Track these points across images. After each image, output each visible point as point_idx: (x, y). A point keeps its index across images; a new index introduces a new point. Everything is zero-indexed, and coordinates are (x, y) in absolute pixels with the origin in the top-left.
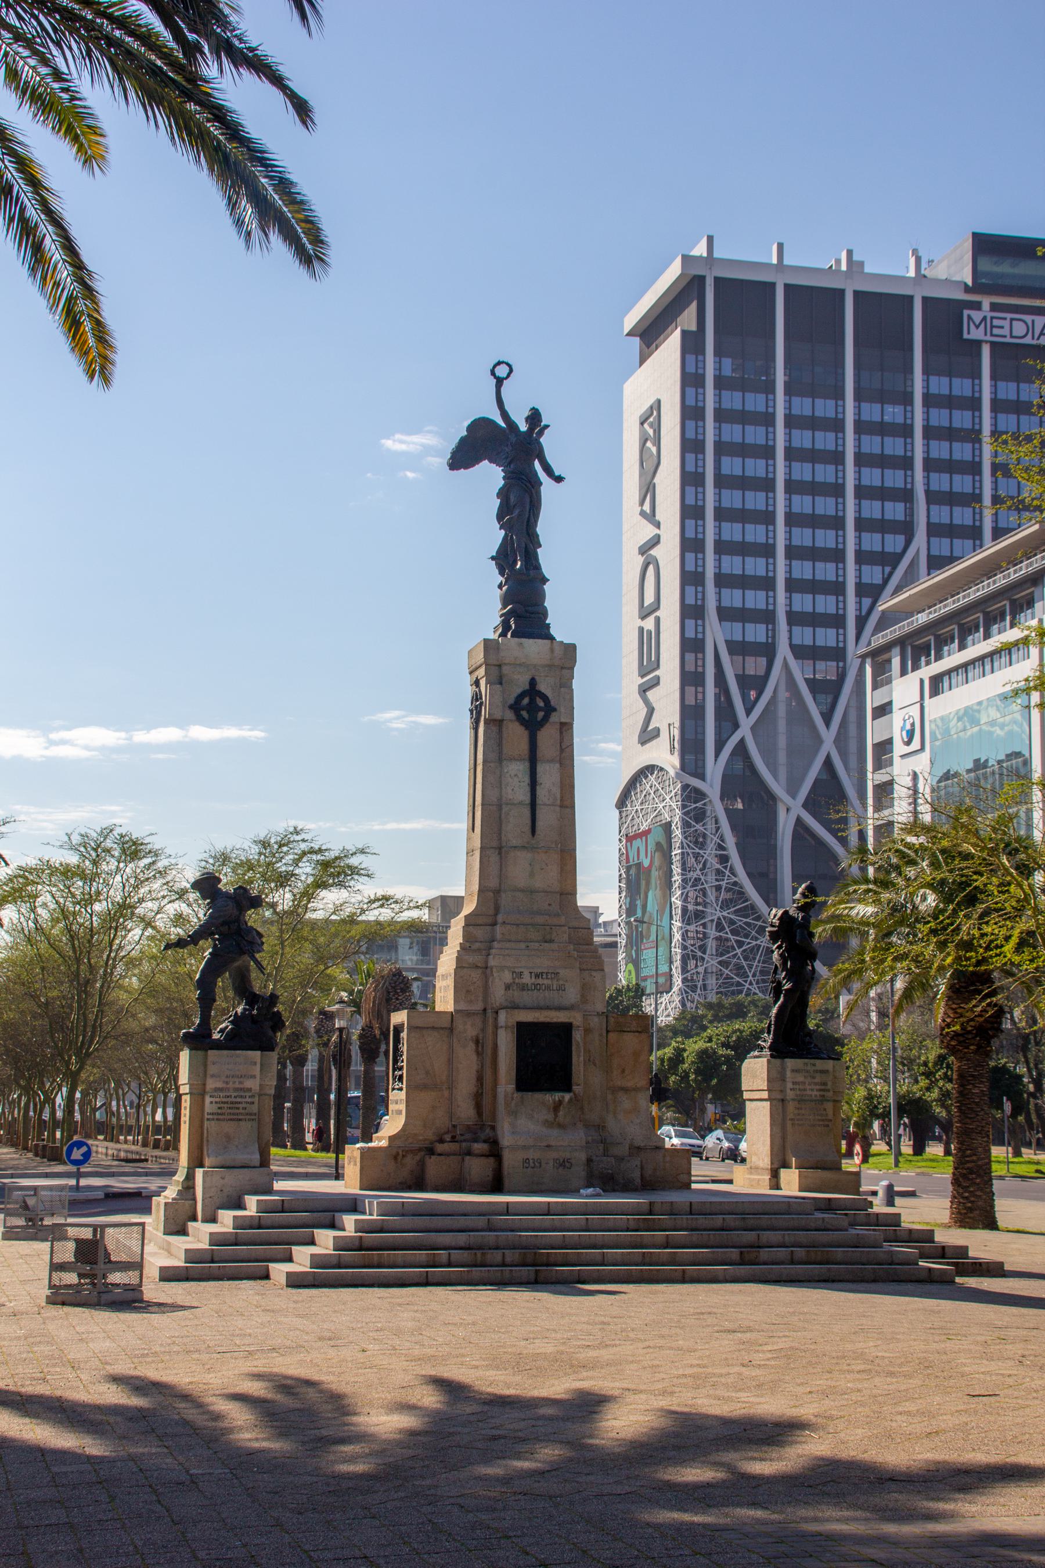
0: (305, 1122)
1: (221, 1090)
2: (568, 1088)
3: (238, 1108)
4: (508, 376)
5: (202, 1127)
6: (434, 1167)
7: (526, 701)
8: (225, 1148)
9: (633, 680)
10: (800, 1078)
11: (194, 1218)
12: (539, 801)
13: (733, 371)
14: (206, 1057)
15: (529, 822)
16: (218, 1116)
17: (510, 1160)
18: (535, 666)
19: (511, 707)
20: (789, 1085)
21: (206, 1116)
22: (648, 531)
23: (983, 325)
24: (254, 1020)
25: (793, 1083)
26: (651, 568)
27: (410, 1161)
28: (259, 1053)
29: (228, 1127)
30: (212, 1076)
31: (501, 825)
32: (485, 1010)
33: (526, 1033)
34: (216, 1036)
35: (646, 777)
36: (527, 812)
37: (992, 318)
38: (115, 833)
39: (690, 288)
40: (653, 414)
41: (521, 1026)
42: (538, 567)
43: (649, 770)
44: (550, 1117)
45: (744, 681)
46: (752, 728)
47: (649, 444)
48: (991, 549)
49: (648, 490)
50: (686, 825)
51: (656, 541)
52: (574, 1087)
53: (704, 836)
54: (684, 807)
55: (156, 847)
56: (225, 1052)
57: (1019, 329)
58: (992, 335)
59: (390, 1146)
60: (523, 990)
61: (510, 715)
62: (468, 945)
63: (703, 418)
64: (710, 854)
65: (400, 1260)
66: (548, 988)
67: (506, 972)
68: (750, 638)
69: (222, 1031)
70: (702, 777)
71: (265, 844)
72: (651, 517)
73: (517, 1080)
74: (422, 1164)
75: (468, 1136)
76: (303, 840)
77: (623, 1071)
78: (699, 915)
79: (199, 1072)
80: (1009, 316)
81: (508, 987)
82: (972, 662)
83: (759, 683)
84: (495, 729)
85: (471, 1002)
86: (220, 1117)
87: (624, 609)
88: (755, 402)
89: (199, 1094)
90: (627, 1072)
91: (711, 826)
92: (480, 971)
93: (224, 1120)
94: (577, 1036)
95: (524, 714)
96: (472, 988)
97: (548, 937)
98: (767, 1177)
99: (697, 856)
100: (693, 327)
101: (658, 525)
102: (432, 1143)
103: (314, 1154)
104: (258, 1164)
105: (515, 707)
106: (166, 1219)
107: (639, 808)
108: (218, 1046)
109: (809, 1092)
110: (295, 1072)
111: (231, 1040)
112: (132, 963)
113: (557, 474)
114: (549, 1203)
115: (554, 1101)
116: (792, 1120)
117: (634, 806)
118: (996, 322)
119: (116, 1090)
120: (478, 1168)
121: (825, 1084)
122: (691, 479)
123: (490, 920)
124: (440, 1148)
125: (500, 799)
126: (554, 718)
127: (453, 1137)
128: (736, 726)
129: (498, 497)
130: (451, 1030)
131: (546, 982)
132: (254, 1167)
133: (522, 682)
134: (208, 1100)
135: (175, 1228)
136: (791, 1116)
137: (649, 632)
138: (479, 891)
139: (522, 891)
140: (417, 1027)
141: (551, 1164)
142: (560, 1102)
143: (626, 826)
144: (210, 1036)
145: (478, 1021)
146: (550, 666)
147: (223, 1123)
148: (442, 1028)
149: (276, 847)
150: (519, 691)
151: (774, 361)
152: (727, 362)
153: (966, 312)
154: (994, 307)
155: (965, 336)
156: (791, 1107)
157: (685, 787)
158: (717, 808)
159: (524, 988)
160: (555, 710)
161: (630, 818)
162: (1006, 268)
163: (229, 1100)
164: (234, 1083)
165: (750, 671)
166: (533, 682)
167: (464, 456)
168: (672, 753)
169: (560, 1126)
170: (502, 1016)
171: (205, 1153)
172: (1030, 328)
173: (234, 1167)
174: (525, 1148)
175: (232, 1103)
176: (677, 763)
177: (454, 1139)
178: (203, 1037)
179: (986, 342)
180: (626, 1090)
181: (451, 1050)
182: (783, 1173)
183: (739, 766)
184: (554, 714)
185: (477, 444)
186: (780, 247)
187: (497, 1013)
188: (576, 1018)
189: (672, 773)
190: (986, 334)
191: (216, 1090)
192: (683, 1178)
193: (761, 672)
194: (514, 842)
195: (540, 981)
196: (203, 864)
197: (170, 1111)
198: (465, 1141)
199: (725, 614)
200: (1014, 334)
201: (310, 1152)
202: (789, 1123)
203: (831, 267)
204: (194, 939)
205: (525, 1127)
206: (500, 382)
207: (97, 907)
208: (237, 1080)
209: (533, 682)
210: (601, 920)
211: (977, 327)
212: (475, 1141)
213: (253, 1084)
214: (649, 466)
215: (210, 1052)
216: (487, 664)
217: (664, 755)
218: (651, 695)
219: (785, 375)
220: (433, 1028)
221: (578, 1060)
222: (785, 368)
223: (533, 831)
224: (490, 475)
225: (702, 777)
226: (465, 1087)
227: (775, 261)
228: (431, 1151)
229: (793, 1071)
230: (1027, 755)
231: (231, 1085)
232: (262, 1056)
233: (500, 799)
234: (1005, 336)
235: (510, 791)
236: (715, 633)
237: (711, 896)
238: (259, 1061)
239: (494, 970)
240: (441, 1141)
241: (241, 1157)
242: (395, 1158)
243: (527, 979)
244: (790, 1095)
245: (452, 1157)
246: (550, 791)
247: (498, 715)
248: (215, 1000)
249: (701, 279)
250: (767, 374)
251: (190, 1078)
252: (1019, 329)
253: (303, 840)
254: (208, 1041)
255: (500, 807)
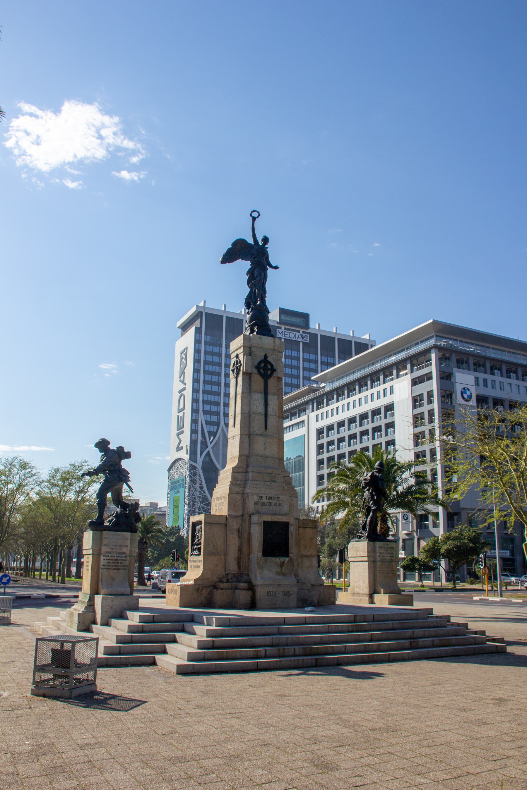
1: (109, 553)
2: (287, 555)
5: (98, 572)
6: (219, 596)
7: (262, 365)
9: (175, 432)
10: (382, 551)
12: (268, 413)
14: (101, 535)
15: (264, 423)
16: (107, 567)
17: (260, 592)
19: (256, 367)
20: (378, 554)
22: (182, 386)
25: (380, 553)
26: (182, 397)
27: (205, 592)
28: (130, 533)
30: (105, 545)
31: (250, 424)
32: (243, 515)
33: (268, 526)
34: (106, 524)
36: (263, 418)
38: (18, 459)
39: (198, 315)
40: (185, 351)
41: (265, 523)
42: (265, 305)
43: (179, 459)
44: (279, 570)
45: (210, 433)
46: (212, 448)
47: (183, 360)
48: (302, 389)
49: (182, 373)
50: (190, 477)
51: (184, 389)
52: (290, 555)
53: (196, 480)
54: (190, 471)
55: (33, 465)
56: (112, 532)
57: (292, 336)
59: (195, 584)
60: (263, 505)
61: (255, 371)
62: (234, 482)
63: (200, 353)
64: (197, 486)
65: (238, 655)
66: (274, 505)
67: (255, 496)
68: (212, 420)
69: (110, 521)
70: (196, 462)
71: (74, 466)
72: (183, 382)
73: (263, 551)
74: (211, 594)
75: (234, 579)
77: (306, 547)
78: (194, 505)
79: (97, 543)
80: (289, 332)
81: (256, 504)
82: (295, 425)
83: (214, 434)
84: (247, 377)
85: (236, 511)
86: (109, 567)
87: (173, 410)
88: (216, 350)
89: (96, 554)
90: (307, 547)
91: (198, 478)
92: (240, 495)
93: (110, 569)
94: (292, 529)
95: (262, 371)
96: (236, 504)
97: (273, 479)
98: (367, 598)
99: (193, 487)
100: (199, 326)
101: (185, 384)
102: (215, 583)
105: (258, 367)
108: (108, 529)
109: (386, 558)
110: (68, 551)
111: (115, 526)
112: (18, 510)
113: (274, 265)
114: (305, 617)
115: (281, 561)
116: (379, 571)
117: (174, 470)
119: (6, 555)
120: (243, 596)
121: (392, 554)
122: (196, 371)
123: (244, 471)
124: (222, 585)
125: (250, 411)
126: (275, 374)
127: (228, 580)
128: (207, 447)
130: (226, 525)
131: (273, 501)
132: (127, 595)
133: (260, 356)
134: (102, 558)
136: (378, 569)
137: (181, 417)
138: (240, 456)
139: (261, 456)
140: (209, 523)
141: (281, 594)
142: (284, 562)
144: (103, 523)
145: (239, 520)
146: (274, 350)
147: (110, 571)
148: (222, 524)
150: (259, 360)
151: (222, 338)
153: (277, 329)
154: (285, 329)
156: (379, 564)
157: (191, 465)
158: (200, 472)
159: (263, 504)
160: (275, 370)
163: (113, 558)
164: (116, 549)
165: (212, 430)
166: (266, 357)
167: (229, 257)
168: (187, 454)
169: (284, 574)
170: (255, 518)
171: (100, 586)
172: (295, 336)
174: (268, 585)
175: (115, 560)
176: (188, 457)
177: (228, 581)
180: (307, 556)
181: (226, 536)
182: (376, 596)
183: (207, 459)
184: (275, 372)
186: (225, 306)
187: (250, 516)
188: (292, 521)
189: (187, 460)
191: (107, 552)
192: (332, 599)
193: (215, 431)
194: (257, 432)
195: (270, 501)
196: (50, 472)
197: (18, 563)
198: (233, 582)
199: (205, 412)
201: (73, 579)
202: (378, 572)
204: (96, 472)
205: (266, 575)
207: (10, 486)
208: (118, 548)
209: (266, 357)
210: (158, 507)
212: (239, 581)
213: (126, 550)
214: (183, 366)
215: (104, 532)
216: (244, 346)
217: (185, 455)
220: (217, 523)
221: (292, 541)
223: (266, 428)
225: (196, 462)
226: (233, 553)
227: (223, 309)
228: (215, 587)
229: (379, 547)
230: (303, 456)
233: (250, 411)
235: (255, 407)
236: (202, 418)
237: (197, 499)
238: (129, 538)
239: (249, 495)
240: (221, 581)
241: (121, 590)
242: (198, 590)
243: (264, 500)
244: (378, 559)
245: (228, 590)
246: (273, 409)
247: (250, 371)
248: (106, 505)
249: (202, 313)
251: (92, 546)
252: (292, 336)
255: (250, 415)
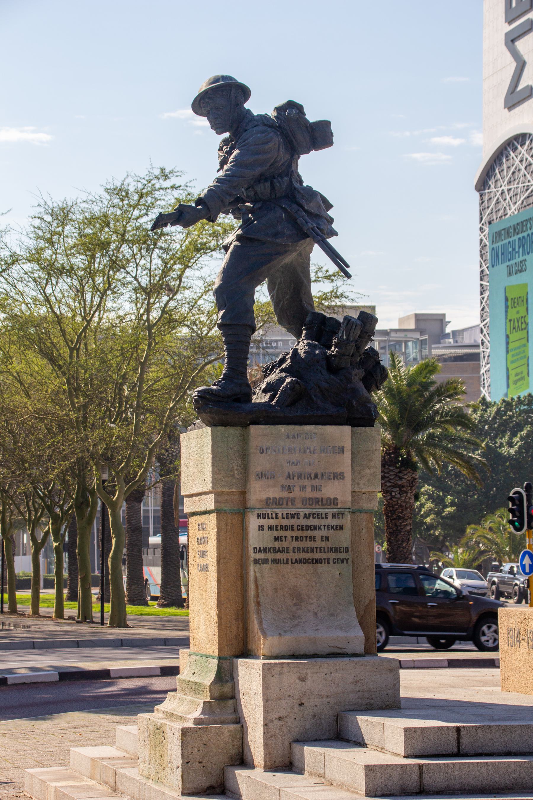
0: (146, 570)
1: (278, 502)
3: (313, 539)
5: (243, 576)
8: (294, 617)
11: (243, 760)
14: (245, 440)
16: (274, 555)
21: (252, 555)
24: (331, 366)
28: (347, 429)
29: (297, 576)
30: (261, 476)
34: (260, 398)
35: (515, 149)
56: (283, 429)
69: (271, 388)
71: (121, 193)
76: (173, 187)
86: (279, 556)
89: (233, 512)
103: (160, 609)
104: (361, 649)
106: (186, 762)
107: (505, 189)
108: (266, 416)
111: (293, 404)
117: (500, 185)
134: (253, 523)
135: (203, 782)
143: (488, 211)
144: (248, 396)
147: (286, 569)
149: (136, 197)
161: (494, 201)
164: (303, 488)
171: (255, 626)
173: (315, 656)
175: (301, 528)
178: (237, 400)
191: (269, 502)
196: (37, 222)
201: (154, 608)
208: (306, 482)
210: (448, 330)
213: (339, 491)
215: (254, 429)
218: (521, 45)
231: (297, 493)
232: (353, 433)
238: (347, 444)
241: (329, 636)
251: (215, 482)
253: (173, 187)
254: (247, 407)
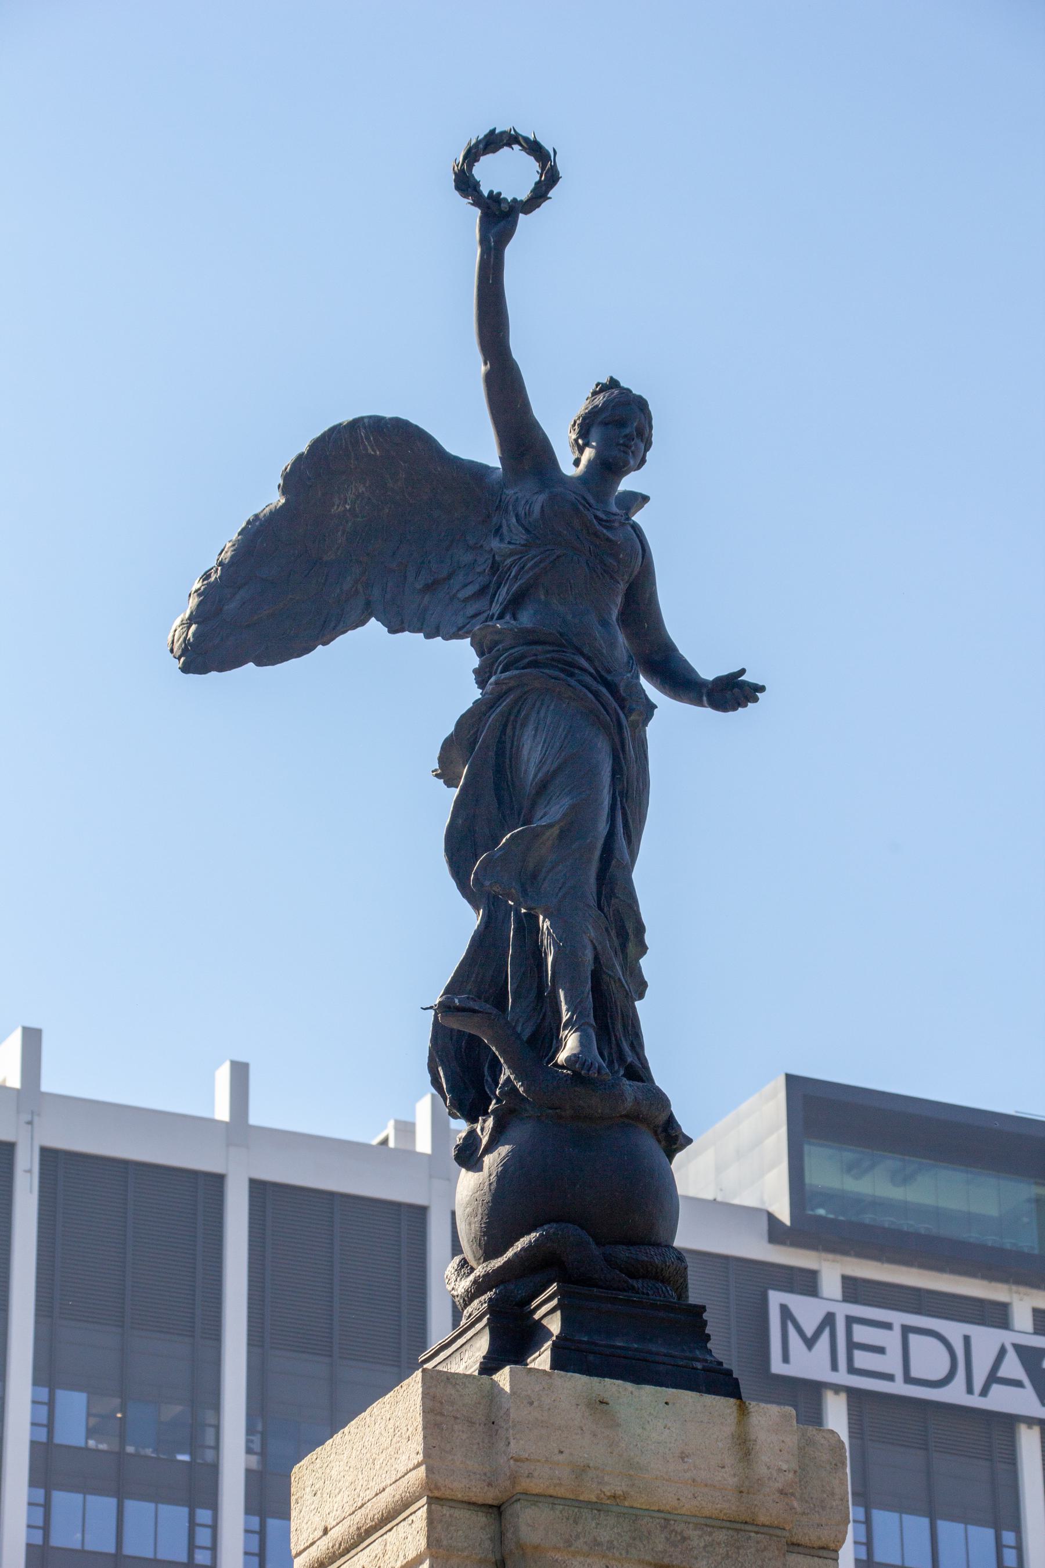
4: (540, 194)
13: (90, 1433)
18: (666, 1518)
23: (826, 1335)
37: (850, 1320)
57: (929, 1358)
58: (852, 1370)
80: (899, 1318)
113: (708, 671)
118: (861, 1334)
129: (446, 773)
151: (216, 1405)
152: (73, 1405)
153: (776, 1298)
154: (855, 1290)
155: (777, 1367)
162: (877, 1185)
167: (260, 606)
172: (959, 1361)
179: (837, 1389)
185: (341, 541)
186: (240, 1073)
190: (834, 1367)
200: (914, 1373)
203: (385, 1142)
206: (498, 219)
211: (810, 1343)
219: (249, 1451)
222: (250, 1430)
224: (403, 688)
227: (222, 1112)
234: (890, 1378)
250: (194, 1445)
252: (929, 1358)
